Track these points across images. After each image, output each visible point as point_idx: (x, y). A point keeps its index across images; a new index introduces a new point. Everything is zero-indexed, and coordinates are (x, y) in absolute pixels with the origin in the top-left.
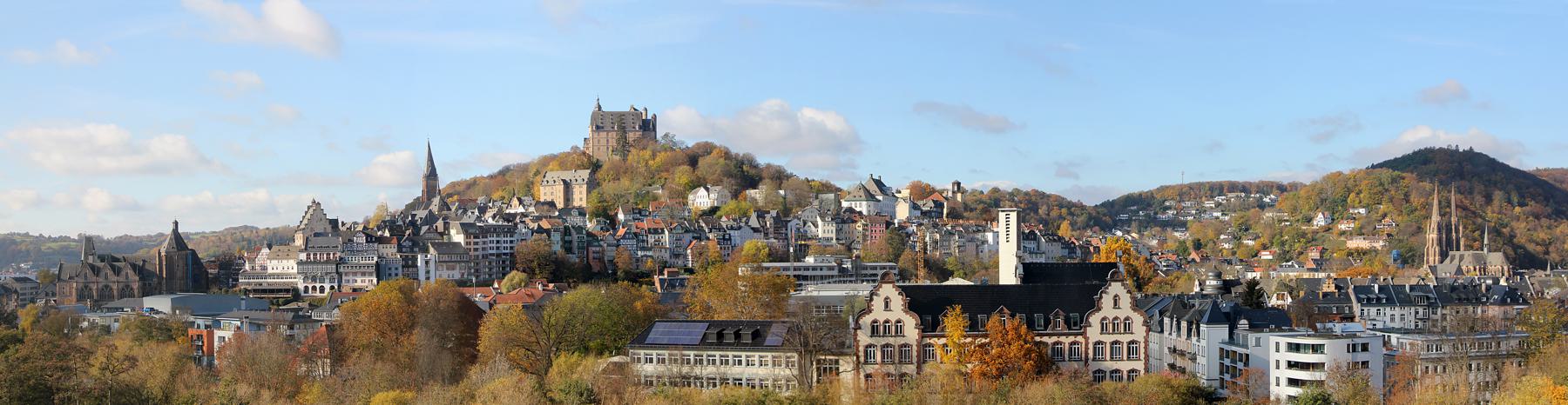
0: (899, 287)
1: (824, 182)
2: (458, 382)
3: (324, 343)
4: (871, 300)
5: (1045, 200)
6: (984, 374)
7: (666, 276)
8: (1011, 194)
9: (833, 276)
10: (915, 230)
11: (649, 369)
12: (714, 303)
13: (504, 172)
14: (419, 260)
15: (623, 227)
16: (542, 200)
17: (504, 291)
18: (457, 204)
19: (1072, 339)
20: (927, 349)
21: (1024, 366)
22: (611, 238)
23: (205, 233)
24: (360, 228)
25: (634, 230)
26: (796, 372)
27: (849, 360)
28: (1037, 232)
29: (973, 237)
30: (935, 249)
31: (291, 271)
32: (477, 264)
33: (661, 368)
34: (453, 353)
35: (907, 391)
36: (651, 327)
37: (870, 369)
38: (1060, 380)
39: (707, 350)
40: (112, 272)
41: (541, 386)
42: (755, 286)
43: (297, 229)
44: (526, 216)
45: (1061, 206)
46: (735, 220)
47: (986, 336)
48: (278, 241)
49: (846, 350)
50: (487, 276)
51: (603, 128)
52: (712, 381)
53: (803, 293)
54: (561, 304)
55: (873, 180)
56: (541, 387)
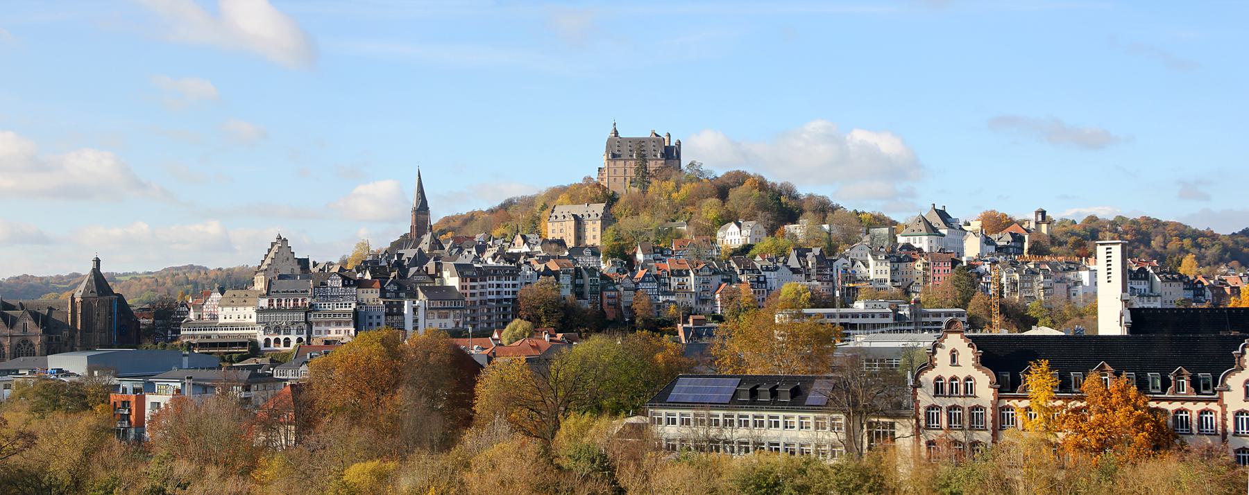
0: (969, 337)
1: (877, 214)
2: (449, 448)
3: (287, 408)
4: (934, 352)
5: (1160, 228)
6: (1080, 446)
7: (691, 325)
8: (1114, 224)
9: (887, 325)
10: (988, 270)
11: (672, 431)
12: (746, 355)
13: (507, 206)
14: (406, 307)
15: (642, 269)
16: (550, 238)
17: (505, 342)
18: (451, 242)
20: (1006, 412)
21: (1136, 439)
22: (628, 281)
23: (137, 274)
24: (336, 269)
25: (655, 272)
26: (842, 436)
27: (908, 424)
28: (1149, 269)
29: (1062, 277)
30: (1014, 291)
31: (248, 320)
32: (474, 311)
33: (685, 430)
34: (444, 415)
35: (979, 464)
36: (673, 383)
37: (932, 435)
38: (1187, 458)
39: (737, 409)
41: (546, 451)
42: (795, 335)
43: (258, 270)
44: (531, 256)
45: (1182, 236)
46: (771, 260)
47: (1082, 399)
49: (903, 412)
50: (485, 325)
51: (619, 156)
52: (744, 446)
53: (851, 345)
54: (571, 357)
55: (936, 210)
56: (547, 453)
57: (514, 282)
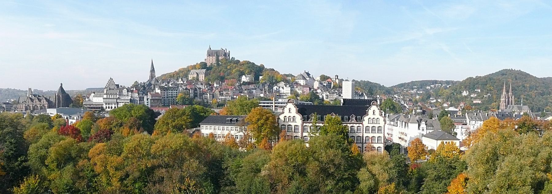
19: (358, 125)
30: (327, 98)
40: (38, 101)
48: (97, 92)
57: (177, 92)
